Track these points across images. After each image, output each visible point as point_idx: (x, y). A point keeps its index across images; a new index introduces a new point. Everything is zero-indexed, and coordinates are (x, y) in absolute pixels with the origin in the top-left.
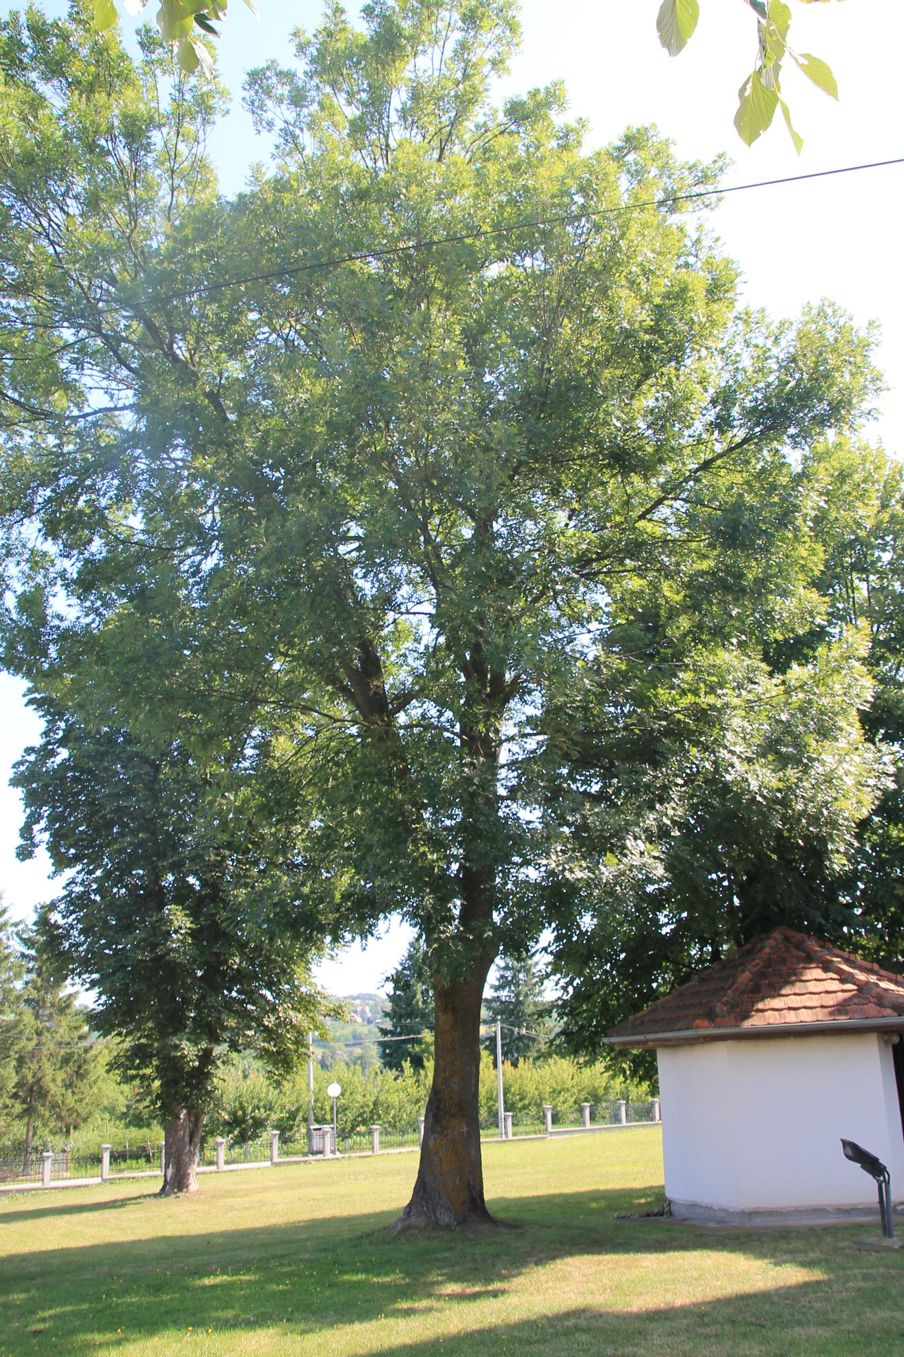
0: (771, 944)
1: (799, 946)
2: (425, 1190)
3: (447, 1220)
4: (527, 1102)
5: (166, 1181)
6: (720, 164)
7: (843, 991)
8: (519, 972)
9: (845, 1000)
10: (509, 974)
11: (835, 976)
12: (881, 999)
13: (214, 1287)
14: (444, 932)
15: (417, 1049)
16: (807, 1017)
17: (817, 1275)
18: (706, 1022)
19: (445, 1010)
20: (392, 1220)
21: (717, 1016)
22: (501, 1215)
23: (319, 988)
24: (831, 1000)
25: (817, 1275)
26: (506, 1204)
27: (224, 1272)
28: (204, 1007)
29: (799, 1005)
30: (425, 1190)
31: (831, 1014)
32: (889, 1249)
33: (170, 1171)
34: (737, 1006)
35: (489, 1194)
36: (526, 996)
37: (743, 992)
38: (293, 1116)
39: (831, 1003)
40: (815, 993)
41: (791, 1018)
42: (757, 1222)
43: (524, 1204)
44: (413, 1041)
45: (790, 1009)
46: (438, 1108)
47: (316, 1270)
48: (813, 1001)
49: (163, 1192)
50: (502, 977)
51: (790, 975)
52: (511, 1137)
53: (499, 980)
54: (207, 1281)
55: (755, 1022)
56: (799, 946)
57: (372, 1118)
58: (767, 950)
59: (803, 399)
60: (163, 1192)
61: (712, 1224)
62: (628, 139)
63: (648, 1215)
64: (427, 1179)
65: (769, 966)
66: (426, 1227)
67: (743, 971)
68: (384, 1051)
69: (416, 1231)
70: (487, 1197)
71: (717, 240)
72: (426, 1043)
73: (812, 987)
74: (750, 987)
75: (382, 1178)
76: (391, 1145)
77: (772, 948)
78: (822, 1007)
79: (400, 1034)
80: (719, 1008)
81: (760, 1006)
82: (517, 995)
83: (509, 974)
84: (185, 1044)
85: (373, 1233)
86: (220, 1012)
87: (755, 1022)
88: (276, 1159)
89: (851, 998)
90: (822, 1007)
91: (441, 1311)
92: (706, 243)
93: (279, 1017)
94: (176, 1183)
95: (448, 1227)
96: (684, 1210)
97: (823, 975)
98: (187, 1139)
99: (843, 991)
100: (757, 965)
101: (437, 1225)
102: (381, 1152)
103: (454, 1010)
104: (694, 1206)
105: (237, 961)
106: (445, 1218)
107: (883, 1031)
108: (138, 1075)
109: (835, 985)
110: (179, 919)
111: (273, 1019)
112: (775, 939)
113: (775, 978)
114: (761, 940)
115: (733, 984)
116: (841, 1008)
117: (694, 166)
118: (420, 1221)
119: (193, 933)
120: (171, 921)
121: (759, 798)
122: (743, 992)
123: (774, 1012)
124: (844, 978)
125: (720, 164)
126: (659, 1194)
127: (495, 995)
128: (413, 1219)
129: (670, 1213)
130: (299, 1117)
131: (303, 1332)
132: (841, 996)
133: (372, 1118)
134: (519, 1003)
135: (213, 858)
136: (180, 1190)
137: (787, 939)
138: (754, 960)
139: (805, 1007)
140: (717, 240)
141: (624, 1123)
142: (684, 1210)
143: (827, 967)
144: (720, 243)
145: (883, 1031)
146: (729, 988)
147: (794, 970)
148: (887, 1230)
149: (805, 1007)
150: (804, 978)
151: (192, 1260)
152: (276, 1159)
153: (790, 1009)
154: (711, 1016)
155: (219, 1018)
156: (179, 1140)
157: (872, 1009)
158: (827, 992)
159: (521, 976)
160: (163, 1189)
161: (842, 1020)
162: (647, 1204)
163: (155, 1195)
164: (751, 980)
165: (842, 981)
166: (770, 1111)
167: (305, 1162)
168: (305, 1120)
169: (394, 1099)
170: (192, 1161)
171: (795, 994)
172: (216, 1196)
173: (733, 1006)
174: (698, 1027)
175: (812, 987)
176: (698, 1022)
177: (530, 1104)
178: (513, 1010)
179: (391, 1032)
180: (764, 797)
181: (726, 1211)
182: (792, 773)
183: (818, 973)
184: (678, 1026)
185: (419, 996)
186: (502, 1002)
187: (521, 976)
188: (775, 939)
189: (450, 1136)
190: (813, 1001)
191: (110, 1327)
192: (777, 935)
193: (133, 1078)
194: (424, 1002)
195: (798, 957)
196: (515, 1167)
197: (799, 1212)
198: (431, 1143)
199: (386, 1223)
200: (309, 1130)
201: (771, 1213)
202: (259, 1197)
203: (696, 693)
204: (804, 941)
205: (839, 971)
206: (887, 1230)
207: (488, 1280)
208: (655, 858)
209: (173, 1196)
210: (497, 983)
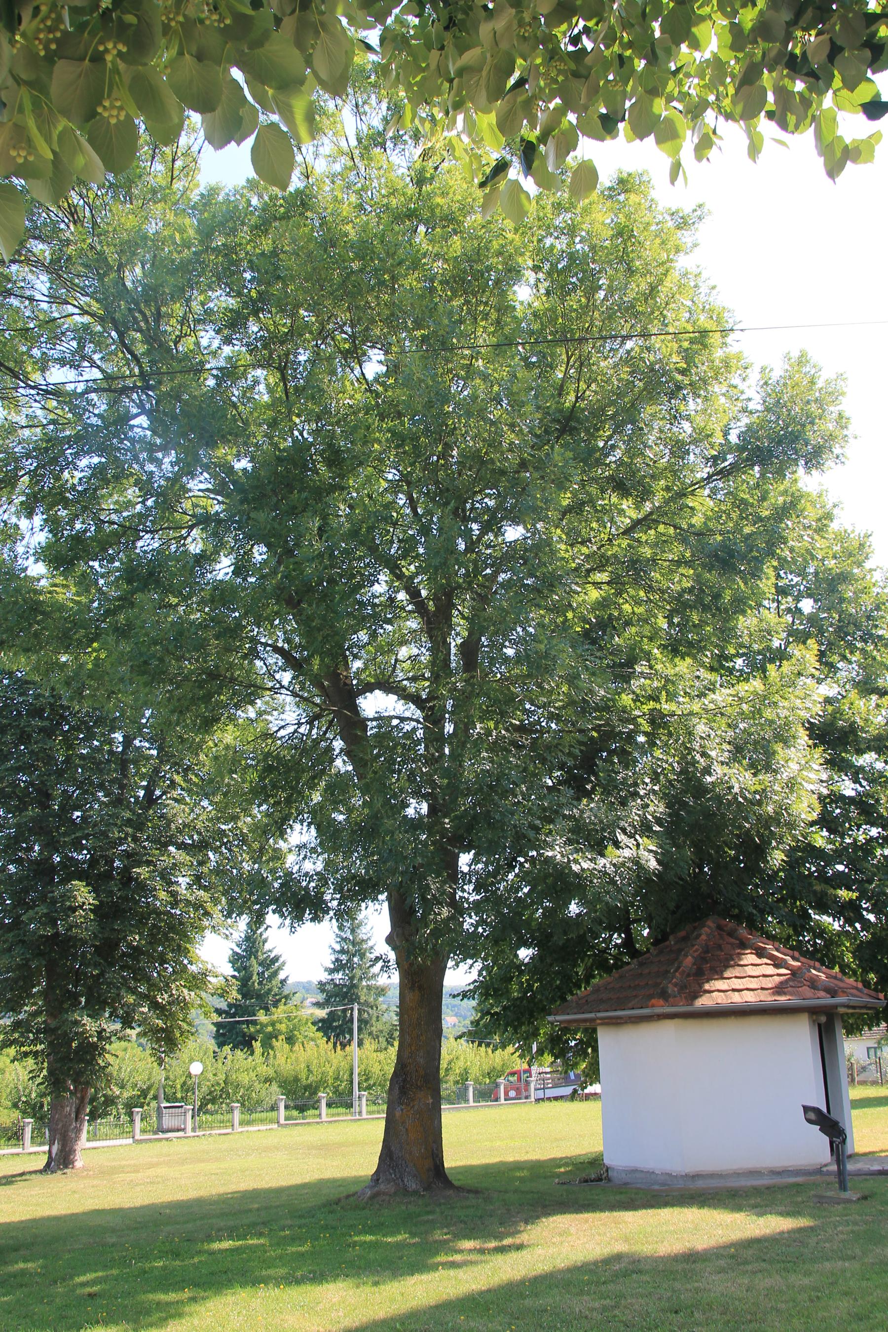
0: (707, 931)
1: (731, 934)
2: (391, 1159)
3: (414, 1186)
4: (372, 1082)
5: (50, 1157)
6: (699, 213)
7: (778, 975)
8: (354, 956)
9: (781, 983)
10: (344, 958)
11: (769, 962)
12: (813, 984)
13: (221, 1251)
14: (439, 914)
15: (252, 1029)
16: (750, 998)
17: (803, 1222)
18: (661, 1002)
19: (412, 988)
20: (357, 1188)
21: (669, 996)
22: (456, 1183)
23: (209, 967)
24: (769, 983)
25: (803, 1222)
26: (468, 1170)
27: (230, 1237)
28: (102, 983)
29: (741, 987)
30: (391, 1159)
31: (774, 994)
32: (849, 1201)
33: (55, 1148)
34: (686, 987)
35: (449, 1162)
36: (361, 979)
37: (689, 975)
38: (144, 1093)
39: (770, 986)
40: (752, 977)
41: (737, 998)
42: (700, 1184)
43: (487, 1171)
44: (248, 1022)
45: (734, 990)
46: (404, 1081)
47: (310, 1233)
48: (753, 983)
49: (48, 1168)
50: (337, 960)
51: (728, 960)
52: (364, 1116)
53: (334, 963)
54: (216, 1246)
55: (703, 1002)
56: (731, 934)
57: (221, 1096)
58: (704, 937)
59: (784, 439)
60: (48, 1168)
61: (656, 1187)
62: (621, 181)
63: (586, 1181)
64: (393, 1148)
65: (707, 952)
66: (395, 1193)
67: (686, 956)
68: (218, 1031)
69: (387, 1198)
70: (446, 1165)
71: (714, 288)
72: (261, 1024)
73: (750, 971)
74: (694, 971)
75: (349, 1145)
76: (249, 1123)
77: (708, 935)
78: (762, 989)
79: (233, 1016)
80: (671, 989)
81: (707, 987)
82: (352, 978)
83: (344, 958)
84: (86, 1020)
85: (339, 1200)
86: (118, 988)
87: (703, 1002)
88: (138, 1137)
89: (787, 981)
90: (762, 989)
91: (486, 1262)
92: (704, 289)
93: (172, 995)
94: (61, 1160)
95: (415, 1193)
96: (624, 1175)
97: (758, 961)
98: (73, 1115)
99: (778, 975)
100: (696, 951)
101: (406, 1192)
102: (240, 1130)
103: (420, 988)
104: (635, 1171)
105: (137, 937)
106: (412, 1185)
107: (813, 1011)
108: (31, 1052)
109: (771, 970)
110: (83, 894)
111: (166, 996)
112: (709, 927)
113: (717, 963)
114: (695, 928)
115: (679, 967)
116: (779, 989)
117: (677, 212)
118: (390, 1188)
119: (96, 910)
120: (75, 897)
121: (740, 799)
122: (689, 975)
123: (720, 992)
124: (778, 964)
125: (699, 213)
126: (596, 1162)
127: (330, 977)
128: (382, 1187)
129: (609, 1179)
130: (150, 1096)
131: (376, 1284)
132: (777, 979)
133: (221, 1096)
134: (354, 986)
135: (117, 835)
136: (66, 1167)
137: (720, 928)
138: (693, 946)
139: (747, 989)
140: (714, 288)
141: (472, 1103)
142: (624, 1175)
143: (760, 953)
144: (714, 292)
145: (813, 1011)
146: (676, 971)
147: (731, 955)
148: (843, 1187)
149: (747, 989)
150: (742, 963)
151: (190, 1226)
152: (138, 1137)
153: (734, 990)
154: (664, 995)
155: (118, 995)
156: (66, 1116)
157: (806, 991)
158: (764, 976)
159: (356, 959)
160: (48, 1165)
161: (782, 999)
162: (566, 1173)
163: (41, 1172)
164: (694, 964)
165: (776, 966)
166: (718, 1084)
167: (167, 1139)
168: (155, 1097)
169: (244, 1078)
170: (77, 1138)
171: (736, 977)
172: (106, 1172)
173: (682, 988)
174: (653, 1006)
175: (750, 971)
176: (653, 1001)
177: (374, 1085)
178: (346, 993)
179: (225, 1012)
180: (745, 798)
181: (669, 1175)
182: (766, 777)
183: (750, 958)
184: (630, 1005)
185: (255, 977)
186: (336, 985)
187: (356, 959)
188: (709, 927)
189: (416, 1107)
190: (753, 983)
191: (179, 1286)
192: (709, 923)
193: (26, 1055)
194: (260, 983)
195: (732, 944)
196: (471, 1137)
197: (737, 1174)
198: (398, 1113)
199: (353, 1189)
200: (159, 1108)
201: (712, 1176)
202: (151, 1172)
203: (656, 699)
204: (736, 930)
205: (771, 957)
206: (843, 1187)
207: (499, 1237)
208: (651, 851)
209: (60, 1172)
210: (332, 966)
